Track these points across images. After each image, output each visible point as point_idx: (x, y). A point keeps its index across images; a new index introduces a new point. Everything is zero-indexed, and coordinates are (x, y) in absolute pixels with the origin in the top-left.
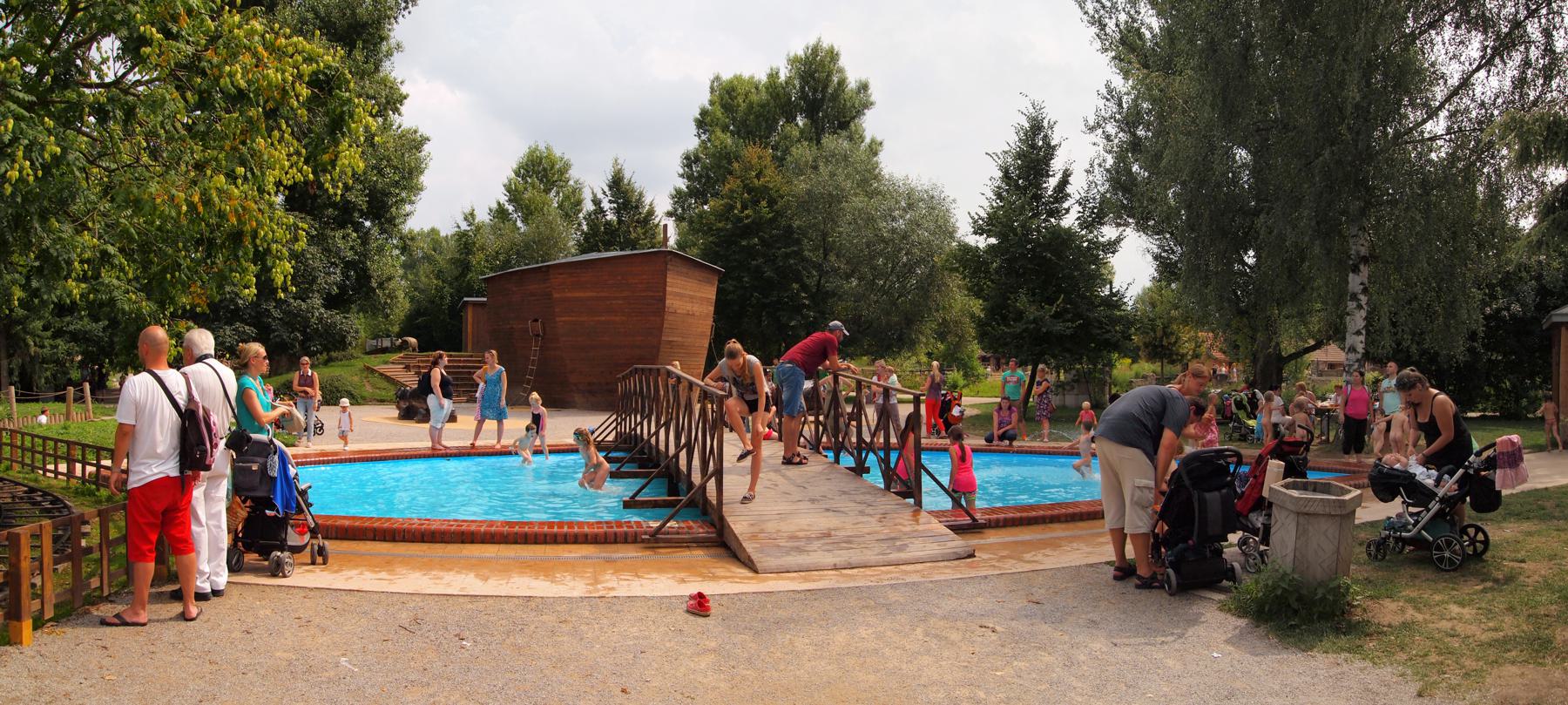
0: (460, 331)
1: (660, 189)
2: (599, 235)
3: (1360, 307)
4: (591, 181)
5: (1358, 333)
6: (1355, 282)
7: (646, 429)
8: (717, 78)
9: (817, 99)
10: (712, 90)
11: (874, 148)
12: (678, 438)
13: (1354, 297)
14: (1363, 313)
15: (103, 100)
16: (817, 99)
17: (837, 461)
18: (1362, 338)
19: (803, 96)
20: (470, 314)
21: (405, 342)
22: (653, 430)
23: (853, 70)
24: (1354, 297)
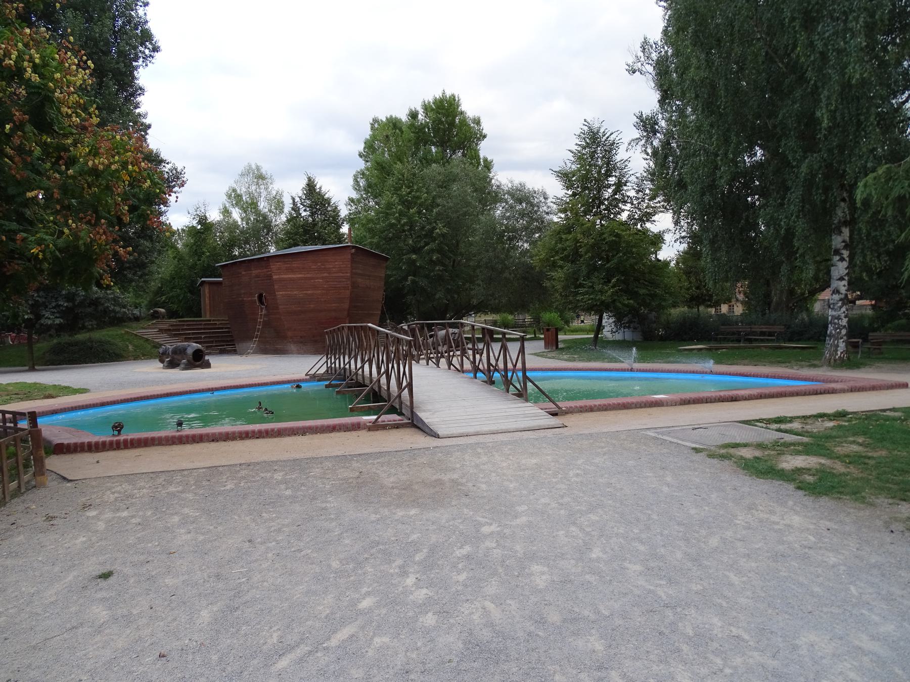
0: (684, 340)
1: (340, 191)
2: (300, 231)
3: (842, 259)
4: (291, 189)
5: (841, 279)
6: (837, 241)
7: (354, 365)
8: (375, 121)
9: (444, 131)
10: (372, 128)
11: (488, 165)
12: (379, 368)
13: (837, 252)
14: (845, 264)
15: (70, 188)
16: (444, 131)
17: (475, 377)
18: (845, 283)
19: (436, 130)
20: (206, 290)
21: (156, 312)
22: (359, 365)
23: (469, 107)
24: (837, 252)
